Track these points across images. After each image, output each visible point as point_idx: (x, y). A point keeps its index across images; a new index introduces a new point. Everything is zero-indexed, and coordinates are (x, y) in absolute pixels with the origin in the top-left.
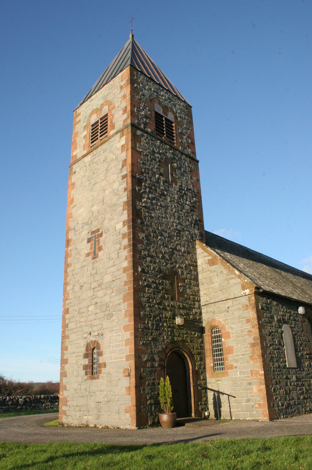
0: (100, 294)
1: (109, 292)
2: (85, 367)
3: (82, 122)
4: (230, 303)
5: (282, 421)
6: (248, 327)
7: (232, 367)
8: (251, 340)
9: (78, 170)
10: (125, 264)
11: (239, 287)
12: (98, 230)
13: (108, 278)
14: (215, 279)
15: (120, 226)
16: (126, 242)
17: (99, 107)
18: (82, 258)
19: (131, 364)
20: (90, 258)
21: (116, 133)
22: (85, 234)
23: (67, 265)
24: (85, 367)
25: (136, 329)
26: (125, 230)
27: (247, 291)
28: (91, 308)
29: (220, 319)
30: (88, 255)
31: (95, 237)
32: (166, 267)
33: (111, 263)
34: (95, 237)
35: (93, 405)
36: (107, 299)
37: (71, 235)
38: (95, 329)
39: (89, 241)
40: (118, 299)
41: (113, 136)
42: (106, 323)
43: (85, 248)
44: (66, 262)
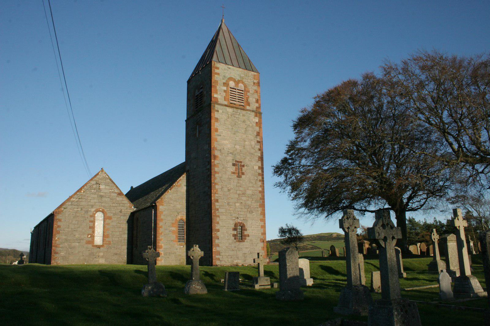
9: (220, 111)
17: (237, 80)
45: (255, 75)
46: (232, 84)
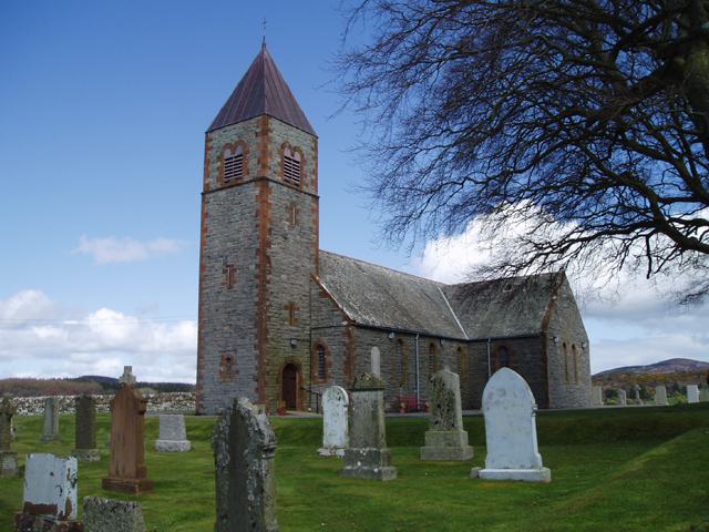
3: (215, 150)
13: (241, 307)
21: (251, 181)
39: (225, 272)
41: (247, 183)
42: (239, 342)
45: (259, 121)
46: (228, 154)
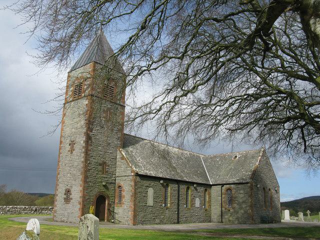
0: (72, 169)
1: (76, 169)
2: (65, 199)
4: (126, 178)
5: (140, 226)
6: (131, 188)
7: (124, 204)
8: (131, 194)
10: (83, 160)
11: (130, 172)
12: (74, 141)
13: (76, 164)
14: (123, 166)
15: (82, 142)
16: (84, 150)
18: (67, 152)
19: (80, 200)
20: (70, 152)
22: (68, 141)
23: (60, 153)
24: (65, 199)
25: (84, 187)
26: (84, 145)
27: (133, 174)
28: (69, 175)
29: (122, 183)
30: (69, 151)
31: (72, 144)
32: (101, 161)
33: (78, 157)
34: (72, 144)
35: (66, 214)
36: (75, 172)
37: (63, 139)
38: (70, 183)
40: (79, 173)
43: (68, 148)
44: (60, 151)
